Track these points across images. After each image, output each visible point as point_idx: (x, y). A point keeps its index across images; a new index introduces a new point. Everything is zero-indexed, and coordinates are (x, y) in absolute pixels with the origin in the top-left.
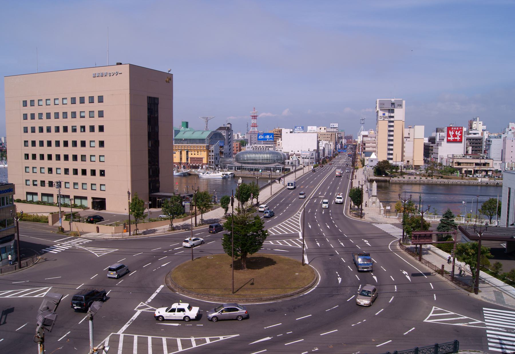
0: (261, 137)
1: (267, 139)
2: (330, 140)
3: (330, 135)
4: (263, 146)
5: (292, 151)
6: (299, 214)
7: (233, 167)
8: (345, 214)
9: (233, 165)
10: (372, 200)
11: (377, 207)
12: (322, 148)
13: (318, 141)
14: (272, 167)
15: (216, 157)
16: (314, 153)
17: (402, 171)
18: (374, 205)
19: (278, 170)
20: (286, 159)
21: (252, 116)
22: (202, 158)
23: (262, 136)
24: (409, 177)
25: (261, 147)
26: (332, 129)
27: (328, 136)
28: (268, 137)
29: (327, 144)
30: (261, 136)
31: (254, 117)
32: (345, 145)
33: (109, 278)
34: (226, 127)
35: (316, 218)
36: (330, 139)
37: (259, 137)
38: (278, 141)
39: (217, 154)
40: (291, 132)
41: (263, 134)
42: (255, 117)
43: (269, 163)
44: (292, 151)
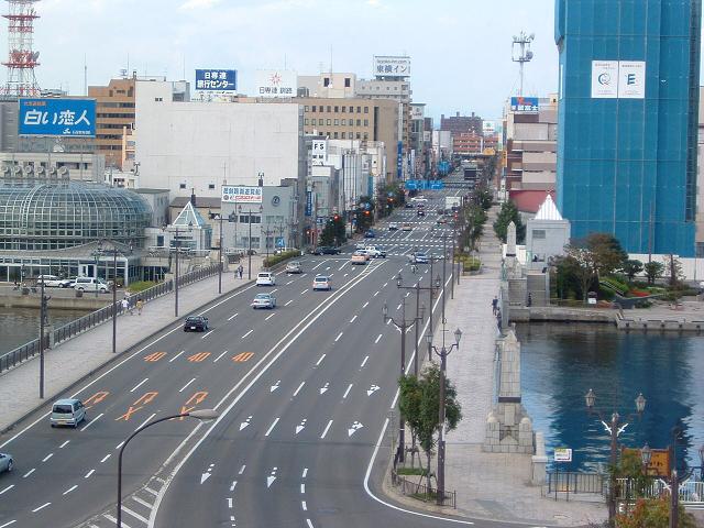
0: (35, 118)
1: (64, 127)
2: (371, 135)
3: (372, 111)
4: (44, 160)
5: (183, 186)
6: (151, 500)
8: (369, 493)
10: (501, 417)
11: (521, 449)
12: (327, 173)
13: (302, 139)
14: (82, 262)
16: (287, 195)
18: (509, 441)
20: (148, 224)
21: (10, 17)
25: (37, 164)
26: (379, 84)
27: (362, 116)
28: (67, 117)
29: (353, 153)
30: (34, 112)
31: (18, 23)
32: (443, 158)
33: (255, 308)
35: (230, 505)
36: (370, 130)
38: (130, 138)
41: (44, 104)
42: (26, 23)
44: (183, 186)
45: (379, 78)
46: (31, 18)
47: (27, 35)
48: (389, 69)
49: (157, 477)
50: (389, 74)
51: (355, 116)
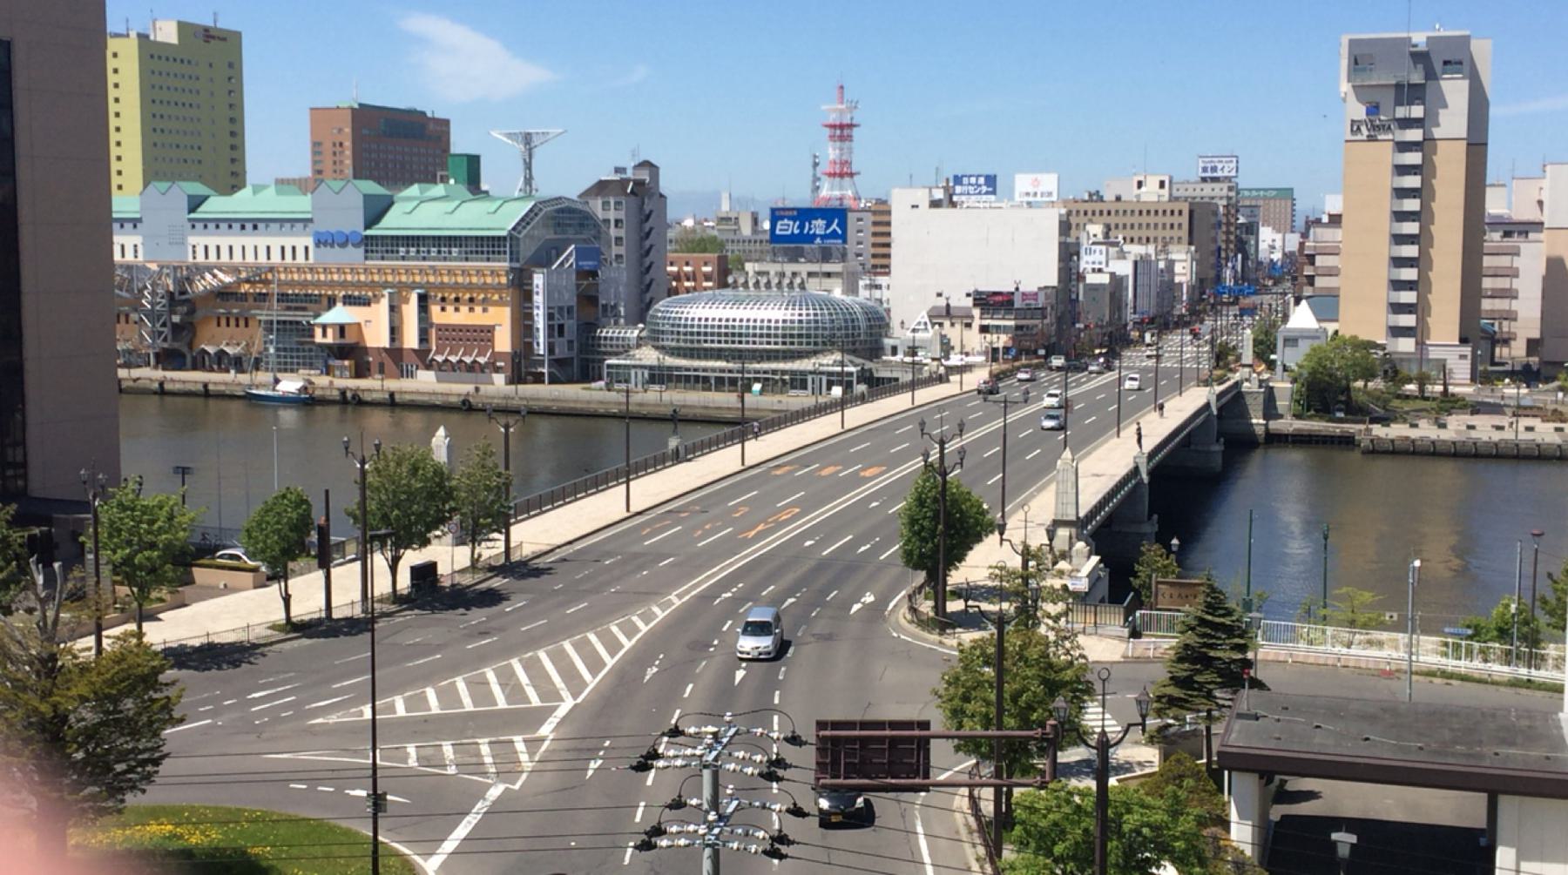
1: (815, 236)
7: (633, 372)
9: (633, 362)
15: (556, 323)
17: (1451, 389)
19: (840, 383)
21: (833, 126)
22: (490, 330)
23: (791, 223)
24: (1470, 423)
26: (1204, 185)
27: (1176, 220)
28: (819, 226)
30: (786, 221)
31: (838, 132)
34: (627, 181)
37: (778, 227)
39: (561, 309)
40: (935, 204)
41: (795, 213)
42: (846, 132)
43: (800, 355)
44: (939, 295)
45: (1204, 180)
46: (851, 126)
47: (847, 143)
48: (1214, 169)
49: (937, 546)
50: (1215, 175)
51: (1168, 220)
